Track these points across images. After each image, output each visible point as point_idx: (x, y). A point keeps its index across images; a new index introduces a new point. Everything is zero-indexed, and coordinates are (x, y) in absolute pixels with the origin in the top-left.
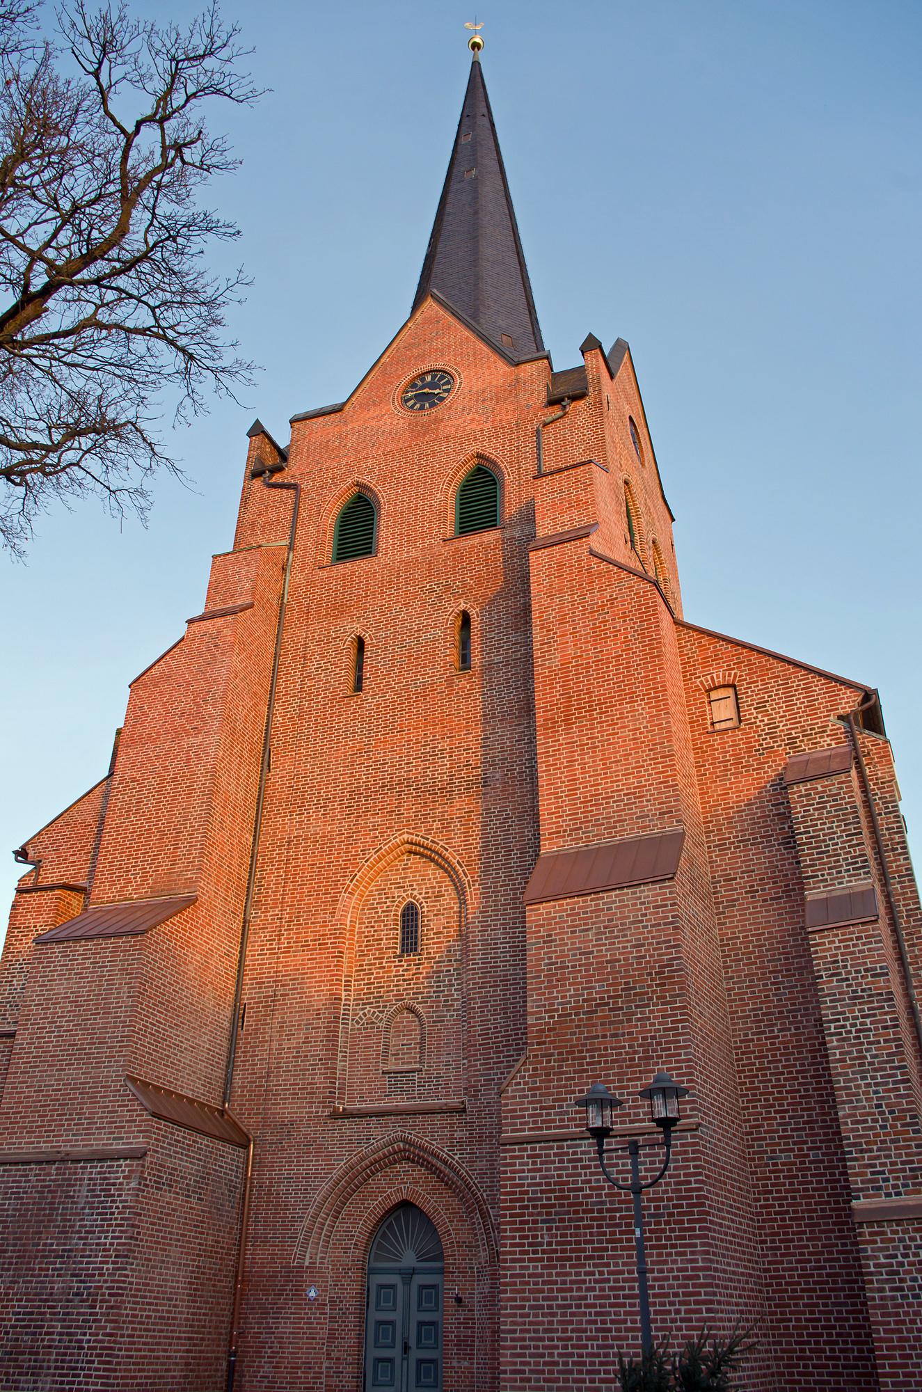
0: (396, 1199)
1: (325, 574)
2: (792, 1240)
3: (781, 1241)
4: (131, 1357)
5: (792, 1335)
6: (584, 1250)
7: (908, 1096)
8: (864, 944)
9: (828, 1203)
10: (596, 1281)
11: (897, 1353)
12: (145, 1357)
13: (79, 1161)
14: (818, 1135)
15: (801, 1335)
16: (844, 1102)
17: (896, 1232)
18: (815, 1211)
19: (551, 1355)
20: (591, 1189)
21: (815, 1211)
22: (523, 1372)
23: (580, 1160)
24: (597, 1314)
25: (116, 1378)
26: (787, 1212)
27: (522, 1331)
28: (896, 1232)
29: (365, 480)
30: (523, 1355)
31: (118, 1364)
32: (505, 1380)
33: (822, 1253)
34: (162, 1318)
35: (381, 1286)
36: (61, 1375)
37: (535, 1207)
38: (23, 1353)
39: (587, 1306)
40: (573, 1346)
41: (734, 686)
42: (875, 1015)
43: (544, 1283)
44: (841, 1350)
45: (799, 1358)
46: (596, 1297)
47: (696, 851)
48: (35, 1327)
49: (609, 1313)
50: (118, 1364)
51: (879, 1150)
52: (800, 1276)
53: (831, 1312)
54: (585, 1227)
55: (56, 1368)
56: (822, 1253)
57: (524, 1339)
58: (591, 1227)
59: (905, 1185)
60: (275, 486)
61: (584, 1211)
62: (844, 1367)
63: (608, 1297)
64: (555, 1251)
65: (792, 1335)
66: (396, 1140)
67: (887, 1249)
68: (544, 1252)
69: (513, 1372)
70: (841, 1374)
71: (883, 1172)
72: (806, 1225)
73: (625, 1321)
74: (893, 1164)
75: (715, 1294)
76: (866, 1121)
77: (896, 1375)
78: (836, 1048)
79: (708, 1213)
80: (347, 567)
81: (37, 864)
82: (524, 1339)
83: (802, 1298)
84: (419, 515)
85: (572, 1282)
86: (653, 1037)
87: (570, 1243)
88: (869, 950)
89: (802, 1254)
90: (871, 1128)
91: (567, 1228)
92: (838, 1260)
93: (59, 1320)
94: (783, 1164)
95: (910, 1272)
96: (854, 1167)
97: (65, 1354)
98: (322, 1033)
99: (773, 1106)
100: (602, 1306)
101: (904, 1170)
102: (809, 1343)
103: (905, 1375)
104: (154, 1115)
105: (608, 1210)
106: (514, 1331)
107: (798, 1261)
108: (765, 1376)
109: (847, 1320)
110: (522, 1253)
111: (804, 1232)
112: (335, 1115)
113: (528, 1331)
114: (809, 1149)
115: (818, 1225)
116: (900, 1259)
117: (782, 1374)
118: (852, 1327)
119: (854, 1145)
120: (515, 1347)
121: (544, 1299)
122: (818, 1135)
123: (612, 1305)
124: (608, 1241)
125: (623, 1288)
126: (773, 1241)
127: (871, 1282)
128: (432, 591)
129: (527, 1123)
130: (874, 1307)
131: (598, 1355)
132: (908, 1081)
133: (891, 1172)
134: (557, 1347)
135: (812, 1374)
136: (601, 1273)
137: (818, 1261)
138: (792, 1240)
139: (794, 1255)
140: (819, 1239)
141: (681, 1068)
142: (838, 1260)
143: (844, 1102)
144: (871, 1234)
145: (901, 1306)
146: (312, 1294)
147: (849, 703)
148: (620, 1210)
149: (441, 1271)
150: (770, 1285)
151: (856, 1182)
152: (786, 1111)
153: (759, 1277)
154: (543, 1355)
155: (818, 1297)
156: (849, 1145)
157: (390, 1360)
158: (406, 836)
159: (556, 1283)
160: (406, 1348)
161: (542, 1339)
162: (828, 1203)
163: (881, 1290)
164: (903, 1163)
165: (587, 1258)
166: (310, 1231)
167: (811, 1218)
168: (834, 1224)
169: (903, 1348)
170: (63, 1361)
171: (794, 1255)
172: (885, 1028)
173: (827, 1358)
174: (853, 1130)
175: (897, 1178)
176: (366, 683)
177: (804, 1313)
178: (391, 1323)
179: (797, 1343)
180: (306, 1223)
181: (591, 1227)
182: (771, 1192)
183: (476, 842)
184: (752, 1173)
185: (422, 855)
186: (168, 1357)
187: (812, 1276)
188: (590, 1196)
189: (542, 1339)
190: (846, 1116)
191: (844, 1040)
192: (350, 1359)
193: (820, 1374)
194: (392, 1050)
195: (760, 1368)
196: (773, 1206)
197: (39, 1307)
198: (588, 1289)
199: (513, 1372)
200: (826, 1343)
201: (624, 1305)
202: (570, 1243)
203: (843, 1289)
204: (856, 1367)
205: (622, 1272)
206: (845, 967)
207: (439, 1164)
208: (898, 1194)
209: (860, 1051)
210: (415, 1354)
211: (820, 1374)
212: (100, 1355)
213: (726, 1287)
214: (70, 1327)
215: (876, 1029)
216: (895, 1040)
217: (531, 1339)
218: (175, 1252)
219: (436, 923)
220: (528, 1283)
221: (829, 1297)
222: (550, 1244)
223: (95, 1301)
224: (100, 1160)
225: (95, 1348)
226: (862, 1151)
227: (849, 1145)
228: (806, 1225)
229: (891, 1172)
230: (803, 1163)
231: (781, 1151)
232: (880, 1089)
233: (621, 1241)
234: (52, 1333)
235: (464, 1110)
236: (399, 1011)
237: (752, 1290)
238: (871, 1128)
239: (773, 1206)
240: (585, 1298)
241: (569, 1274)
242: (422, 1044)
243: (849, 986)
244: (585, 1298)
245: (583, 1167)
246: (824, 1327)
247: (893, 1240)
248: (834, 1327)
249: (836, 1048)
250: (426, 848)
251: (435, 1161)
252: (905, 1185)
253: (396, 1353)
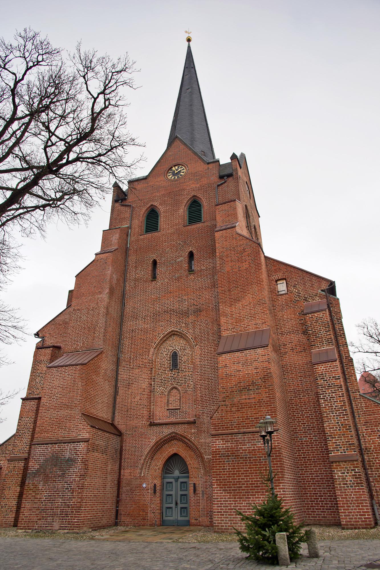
0: (172, 453)
1: (142, 237)
2: (308, 467)
3: (304, 467)
4: (86, 510)
5: (308, 499)
6: (241, 471)
7: (347, 419)
8: (332, 368)
9: (320, 454)
10: (245, 481)
11: (345, 505)
12: (90, 509)
13: (66, 443)
14: (316, 431)
15: (312, 499)
16: (326, 421)
17: (344, 465)
18: (316, 457)
19: (231, 506)
20: (243, 450)
21: (316, 457)
22: (221, 512)
23: (239, 441)
24: (246, 492)
25: (81, 517)
26: (306, 457)
27: (220, 498)
28: (344, 465)
29: (155, 204)
30: (221, 506)
31: (82, 512)
32: (215, 515)
33: (318, 471)
34: (95, 496)
35: (168, 483)
36: (62, 517)
37: (224, 456)
38: (49, 510)
39: (242, 490)
40: (238, 503)
41: (285, 279)
42: (336, 392)
43: (228, 482)
44: (325, 504)
45: (311, 506)
46: (245, 487)
47: (274, 336)
48: (52, 500)
49: (250, 492)
50: (82, 512)
51: (338, 437)
52: (311, 479)
53: (322, 491)
54: (241, 463)
55: (60, 514)
56: (318, 471)
57: (221, 501)
58: (243, 463)
59: (347, 449)
60: (123, 205)
61: (241, 458)
62: (326, 509)
63: (249, 487)
64: (231, 471)
65: (308, 499)
66: (172, 433)
67: (342, 471)
68: (227, 472)
69: (218, 512)
70: (325, 512)
71: (339, 445)
72: (313, 462)
73: (255, 495)
74: (343, 442)
75: (285, 486)
76: (333, 428)
77: (345, 513)
78: (323, 403)
79: (282, 459)
80: (149, 235)
81: (43, 337)
82: (221, 501)
83: (312, 486)
84: (173, 217)
85: (237, 482)
86: (262, 399)
87: (236, 469)
88: (334, 370)
89: (311, 471)
90: (336, 430)
91: (235, 463)
92: (323, 473)
93: (60, 498)
94: (305, 441)
95: (349, 478)
96: (330, 443)
97: (63, 509)
98: (146, 396)
99: (301, 422)
100: (248, 490)
101: (346, 444)
102: (314, 501)
103: (348, 513)
104: (92, 426)
105: (249, 458)
106: (218, 498)
107: (310, 474)
108: (300, 512)
109: (327, 493)
110: (219, 472)
111: (312, 464)
112: (152, 424)
113: (222, 498)
114: (313, 436)
115: (317, 462)
116: (346, 474)
117: (306, 512)
118: (329, 496)
119: (330, 436)
120: (218, 504)
121: (228, 487)
122: (316, 431)
123: (251, 490)
124: (249, 468)
125: (254, 484)
126: (301, 467)
127: (336, 482)
128: (180, 244)
129: (220, 428)
130: (337, 490)
131: (246, 506)
132: (347, 414)
133: (342, 445)
134: (232, 504)
135: (315, 512)
136: (247, 479)
137: (317, 474)
138: (308, 467)
139: (309, 472)
140: (317, 467)
141: (272, 410)
142: (323, 473)
143: (326, 421)
144: (336, 465)
145: (347, 490)
146: (144, 486)
147: (325, 286)
148: (253, 457)
149: (188, 477)
150: (301, 482)
151: (331, 448)
152: (305, 423)
153: (297, 479)
154: (228, 506)
155: (317, 486)
156: (328, 436)
157: (171, 508)
158: (173, 329)
159: (231, 482)
160: (176, 504)
161: (227, 501)
162: (320, 454)
163: (340, 484)
164: (346, 442)
165: (242, 474)
166: (143, 464)
167: (314, 459)
168: (322, 461)
169: (348, 504)
170: (63, 512)
171: (309, 472)
172: (340, 397)
173: (321, 506)
174: (329, 431)
175: (344, 447)
176: (158, 276)
177: (312, 491)
178: (171, 495)
179: (310, 501)
180: (142, 461)
181: (243, 463)
182: (300, 451)
183: (197, 331)
184: (294, 444)
185: (179, 335)
186: (97, 509)
187: (315, 479)
188: (242, 453)
189: (227, 501)
190: (326, 426)
191: (326, 400)
192: (158, 508)
193: (318, 512)
194: (170, 402)
195: (299, 510)
196: (301, 455)
197: (54, 493)
198: (242, 484)
199: (218, 512)
200: (320, 501)
201: (255, 489)
202: (236, 469)
203: (325, 483)
204: (330, 509)
205: (254, 478)
206: (326, 376)
207: (187, 441)
208: (345, 452)
209: (331, 404)
210: (180, 505)
211: (318, 512)
212: (76, 510)
213: (288, 483)
214: (64, 500)
215: (337, 397)
216: (343, 401)
217: (223, 501)
218: (99, 473)
219: (184, 359)
220: (222, 482)
221: (321, 486)
222: (229, 469)
223: (73, 491)
224: (73, 442)
225: (74, 507)
226: (332, 438)
227: (328, 436)
228: (313, 462)
229: (342, 445)
230: (311, 441)
231: (304, 437)
232: (338, 417)
233: (253, 468)
234: (58, 502)
235: (195, 423)
236: (172, 389)
237: (295, 484)
238: (336, 430)
239: (301, 455)
240: (242, 487)
241: (236, 479)
242: (180, 400)
243: (327, 382)
244: (242, 487)
245: (240, 443)
246: (319, 496)
247: (343, 468)
248: (323, 496)
249: (323, 403)
250: (180, 333)
251: (185, 440)
252: (347, 449)
253: (173, 505)
